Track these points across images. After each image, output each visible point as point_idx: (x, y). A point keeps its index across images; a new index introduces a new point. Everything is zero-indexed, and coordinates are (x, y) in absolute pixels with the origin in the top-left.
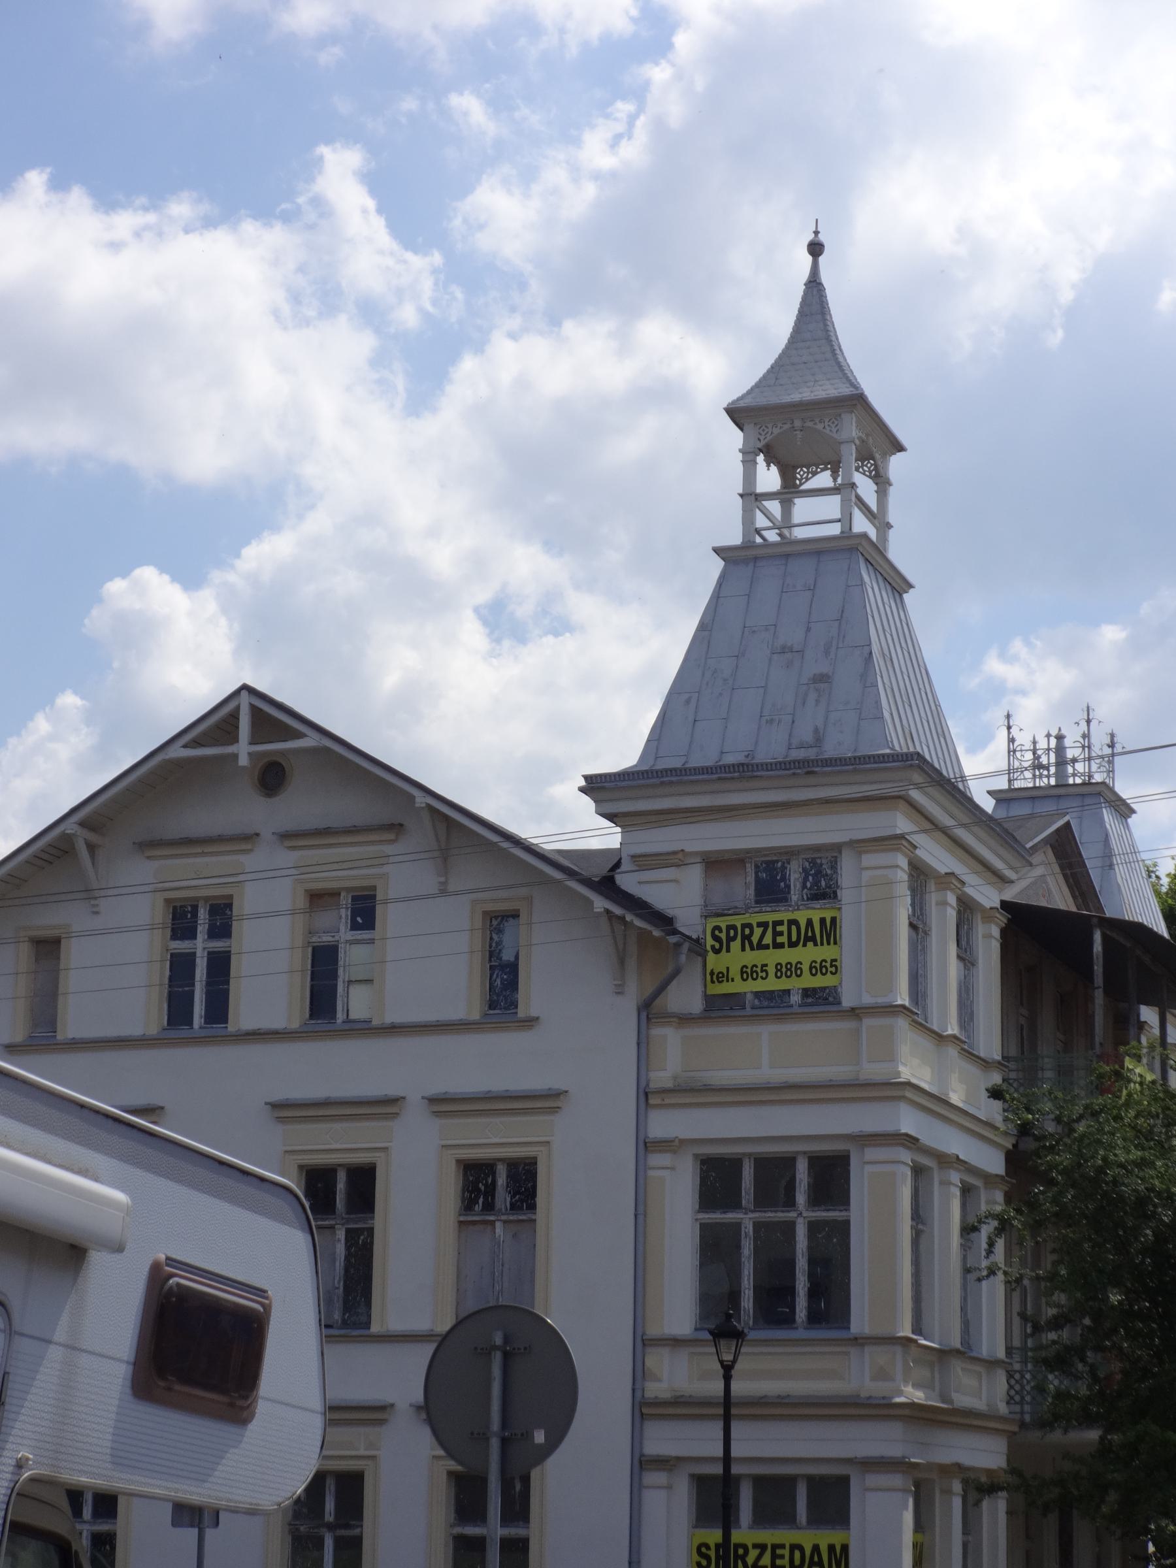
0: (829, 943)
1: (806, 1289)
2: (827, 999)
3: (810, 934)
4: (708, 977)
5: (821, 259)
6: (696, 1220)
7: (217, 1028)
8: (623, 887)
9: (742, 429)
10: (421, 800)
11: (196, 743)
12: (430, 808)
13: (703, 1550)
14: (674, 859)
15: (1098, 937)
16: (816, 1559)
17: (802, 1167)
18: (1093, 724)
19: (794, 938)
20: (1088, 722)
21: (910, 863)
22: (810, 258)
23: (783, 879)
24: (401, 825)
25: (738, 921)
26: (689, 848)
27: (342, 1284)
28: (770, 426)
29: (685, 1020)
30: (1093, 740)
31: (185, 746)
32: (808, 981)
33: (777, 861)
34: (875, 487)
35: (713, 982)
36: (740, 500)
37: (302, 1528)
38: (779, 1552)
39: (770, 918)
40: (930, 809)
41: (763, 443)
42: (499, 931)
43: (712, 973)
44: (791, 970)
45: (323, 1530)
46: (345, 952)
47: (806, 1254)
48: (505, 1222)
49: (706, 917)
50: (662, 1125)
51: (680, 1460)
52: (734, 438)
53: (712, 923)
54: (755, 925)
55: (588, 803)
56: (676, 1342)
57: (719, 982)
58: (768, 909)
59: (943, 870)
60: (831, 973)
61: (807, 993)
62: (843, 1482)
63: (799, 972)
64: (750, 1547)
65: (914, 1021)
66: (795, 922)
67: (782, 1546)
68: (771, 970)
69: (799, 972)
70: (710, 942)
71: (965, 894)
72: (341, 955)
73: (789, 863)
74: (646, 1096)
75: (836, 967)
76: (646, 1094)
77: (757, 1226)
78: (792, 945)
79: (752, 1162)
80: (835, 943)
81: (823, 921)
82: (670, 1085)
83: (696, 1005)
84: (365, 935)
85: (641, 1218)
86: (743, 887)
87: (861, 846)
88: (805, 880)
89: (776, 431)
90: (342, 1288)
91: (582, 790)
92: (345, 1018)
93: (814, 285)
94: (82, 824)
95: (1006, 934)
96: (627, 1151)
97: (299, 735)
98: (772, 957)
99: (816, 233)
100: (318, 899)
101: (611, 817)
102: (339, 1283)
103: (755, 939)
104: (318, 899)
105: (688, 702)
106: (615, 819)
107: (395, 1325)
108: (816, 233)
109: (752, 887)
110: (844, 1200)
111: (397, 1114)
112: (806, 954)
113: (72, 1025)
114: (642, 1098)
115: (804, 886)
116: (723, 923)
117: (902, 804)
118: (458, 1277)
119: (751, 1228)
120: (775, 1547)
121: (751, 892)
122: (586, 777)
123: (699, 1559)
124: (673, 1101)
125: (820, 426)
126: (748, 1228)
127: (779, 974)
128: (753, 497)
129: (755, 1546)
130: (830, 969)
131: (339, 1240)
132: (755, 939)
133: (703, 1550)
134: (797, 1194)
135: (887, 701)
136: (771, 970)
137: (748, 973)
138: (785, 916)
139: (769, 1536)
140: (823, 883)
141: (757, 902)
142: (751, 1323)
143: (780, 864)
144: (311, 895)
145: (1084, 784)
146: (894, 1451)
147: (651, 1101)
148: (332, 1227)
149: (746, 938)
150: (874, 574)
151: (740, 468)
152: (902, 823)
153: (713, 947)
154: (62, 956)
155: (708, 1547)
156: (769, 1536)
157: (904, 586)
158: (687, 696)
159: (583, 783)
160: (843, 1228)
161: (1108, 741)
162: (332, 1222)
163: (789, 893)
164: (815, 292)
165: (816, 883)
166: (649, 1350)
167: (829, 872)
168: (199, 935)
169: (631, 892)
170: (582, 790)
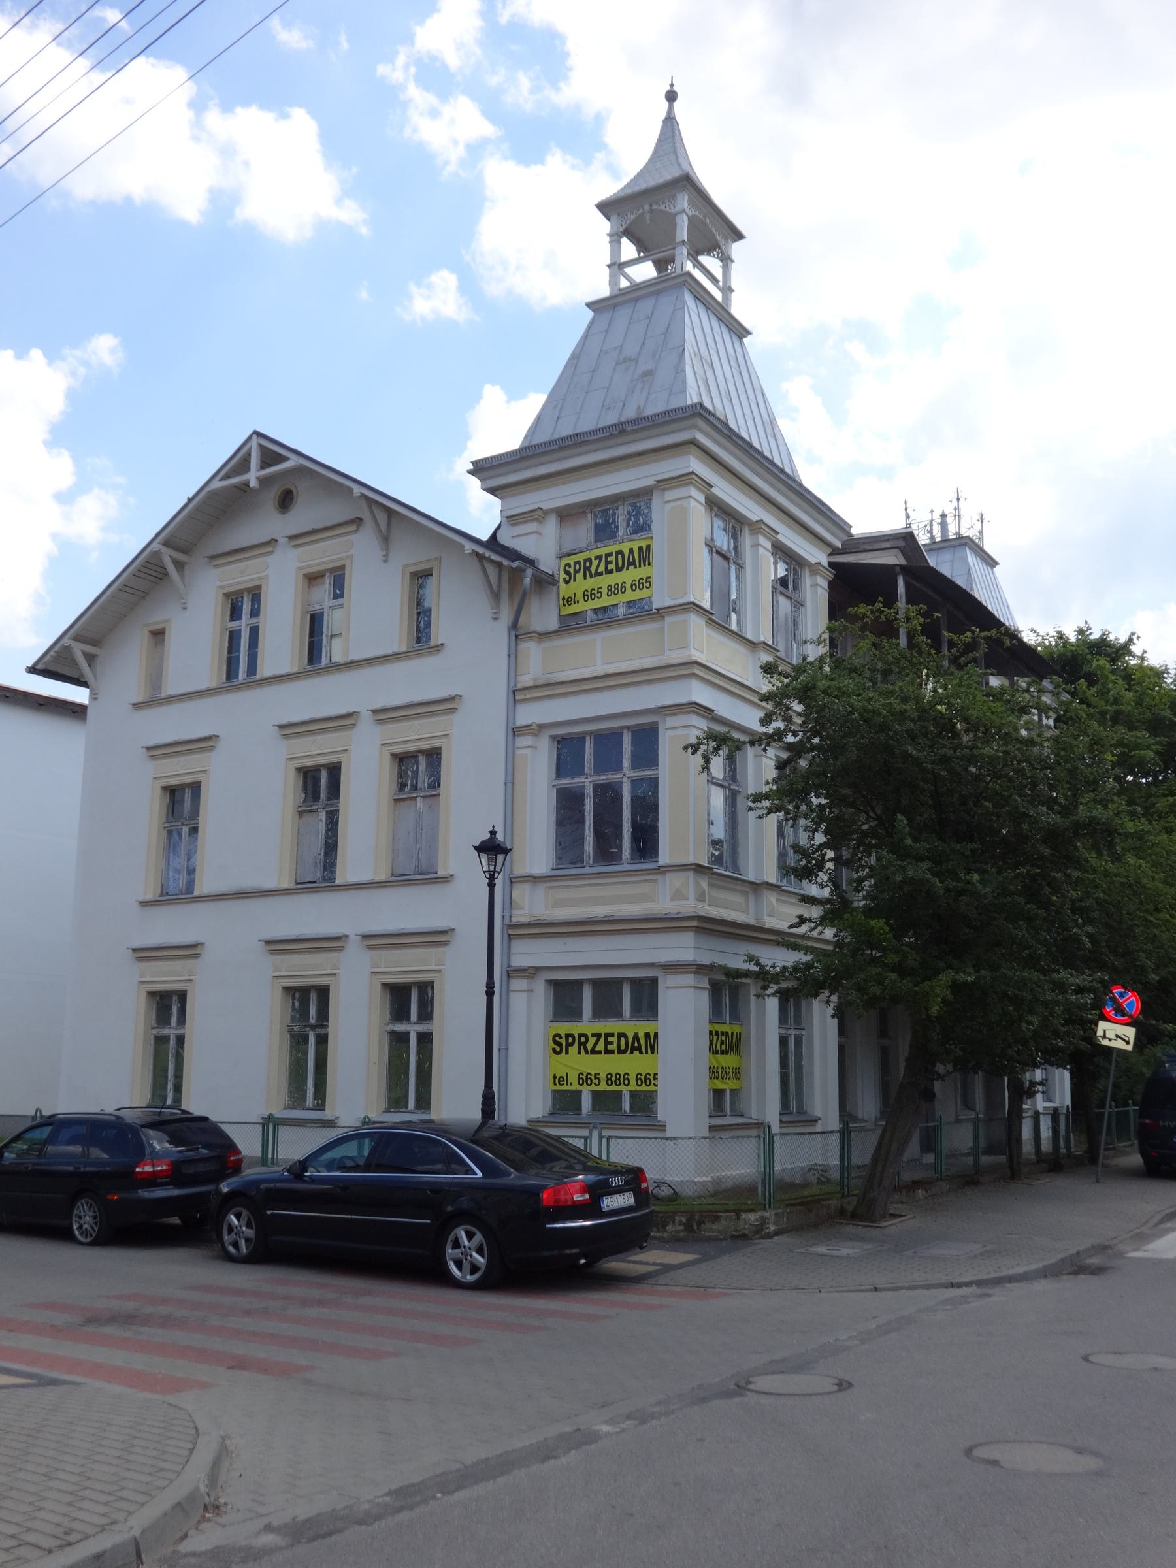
0: (645, 565)
1: (630, 833)
2: (643, 608)
3: (631, 560)
4: (561, 602)
5: (675, 104)
6: (553, 786)
7: (252, 679)
8: (502, 542)
9: (609, 220)
10: (357, 490)
11: (227, 476)
12: (363, 496)
13: (557, 1039)
14: (537, 515)
15: (901, 582)
16: (636, 1045)
17: (627, 739)
18: (985, 521)
19: (620, 565)
20: (958, 499)
21: (707, 498)
22: (667, 104)
23: (614, 521)
24: (361, 519)
25: (581, 557)
26: (545, 506)
27: (323, 851)
28: (629, 214)
29: (544, 636)
30: (962, 512)
31: (221, 480)
32: (630, 596)
33: (609, 509)
34: (721, 264)
35: (564, 605)
36: (607, 269)
37: (295, 1029)
38: (610, 1039)
39: (603, 551)
40: (727, 459)
41: (624, 227)
42: (421, 586)
43: (564, 599)
44: (619, 589)
45: (308, 1029)
46: (329, 615)
47: (630, 806)
48: (423, 797)
49: (560, 557)
50: (528, 714)
51: (538, 969)
52: (604, 226)
53: (564, 561)
54: (593, 559)
55: (475, 482)
56: (535, 879)
57: (569, 605)
58: (602, 545)
59: (754, 518)
60: (646, 587)
61: (629, 604)
62: (654, 981)
63: (623, 590)
64: (589, 1036)
65: (710, 619)
66: (620, 552)
67: (612, 1035)
68: (604, 591)
69: (623, 590)
70: (563, 575)
71: (778, 540)
72: (325, 617)
73: (617, 509)
74: (516, 695)
75: (650, 582)
76: (514, 692)
77: (597, 787)
78: (619, 569)
79: (593, 737)
80: (649, 564)
81: (640, 549)
82: (531, 684)
83: (554, 624)
84: (339, 601)
85: (509, 786)
86: (584, 531)
87: (665, 484)
88: (629, 520)
89: (633, 217)
90: (323, 854)
91: (470, 472)
92: (328, 661)
93: (670, 121)
94: (166, 544)
95: (834, 587)
96: (499, 735)
97: (286, 459)
98: (605, 581)
99: (672, 85)
100: (313, 579)
101: (492, 491)
102: (321, 850)
103: (593, 569)
104: (313, 579)
105: (556, 407)
106: (496, 493)
107: (352, 878)
108: (672, 85)
109: (592, 531)
110: (653, 762)
111: (355, 725)
112: (629, 576)
113: (171, 687)
114: (511, 695)
115: (628, 525)
116: (571, 560)
117: (693, 449)
118: (393, 839)
119: (591, 790)
120: (607, 1035)
121: (592, 534)
122: (473, 463)
123: (554, 1046)
124: (532, 695)
125: (662, 207)
126: (589, 790)
127: (610, 593)
128: (616, 267)
129: (593, 1035)
130: (645, 585)
131: (321, 820)
132: (593, 569)
133: (557, 1039)
134: (624, 760)
135: (757, 438)
136: (604, 591)
137: (588, 595)
138: (613, 549)
139: (603, 1027)
140: (641, 520)
141: (596, 541)
142: (591, 862)
143: (611, 511)
144: (310, 579)
145: (957, 538)
146: (688, 956)
147: (517, 698)
148: (316, 811)
149: (587, 569)
150: (739, 344)
151: (608, 247)
152: (696, 464)
153: (564, 579)
154: (166, 642)
155: (559, 1036)
156: (603, 1027)
157: (744, 333)
158: (555, 403)
159: (471, 467)
160: (654, 783)
161: (979, 518)
162: (317, 807)
163: (618, 531)
164: (669, 124)
165: (637, 521)
166: (515, 886)
167: (645, 511)
168: (244, 617)
169: (506, 545)
170: (470, 472)
